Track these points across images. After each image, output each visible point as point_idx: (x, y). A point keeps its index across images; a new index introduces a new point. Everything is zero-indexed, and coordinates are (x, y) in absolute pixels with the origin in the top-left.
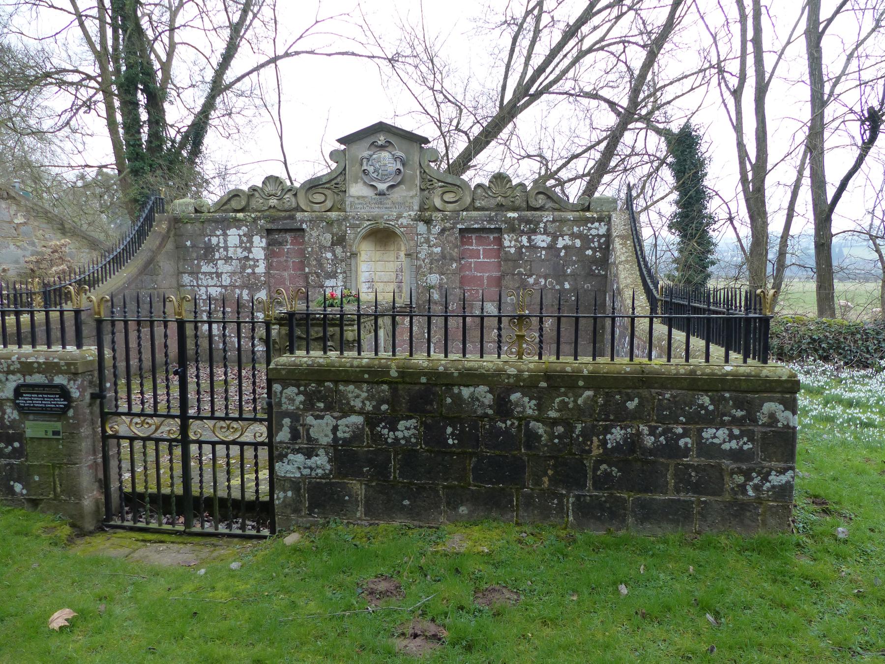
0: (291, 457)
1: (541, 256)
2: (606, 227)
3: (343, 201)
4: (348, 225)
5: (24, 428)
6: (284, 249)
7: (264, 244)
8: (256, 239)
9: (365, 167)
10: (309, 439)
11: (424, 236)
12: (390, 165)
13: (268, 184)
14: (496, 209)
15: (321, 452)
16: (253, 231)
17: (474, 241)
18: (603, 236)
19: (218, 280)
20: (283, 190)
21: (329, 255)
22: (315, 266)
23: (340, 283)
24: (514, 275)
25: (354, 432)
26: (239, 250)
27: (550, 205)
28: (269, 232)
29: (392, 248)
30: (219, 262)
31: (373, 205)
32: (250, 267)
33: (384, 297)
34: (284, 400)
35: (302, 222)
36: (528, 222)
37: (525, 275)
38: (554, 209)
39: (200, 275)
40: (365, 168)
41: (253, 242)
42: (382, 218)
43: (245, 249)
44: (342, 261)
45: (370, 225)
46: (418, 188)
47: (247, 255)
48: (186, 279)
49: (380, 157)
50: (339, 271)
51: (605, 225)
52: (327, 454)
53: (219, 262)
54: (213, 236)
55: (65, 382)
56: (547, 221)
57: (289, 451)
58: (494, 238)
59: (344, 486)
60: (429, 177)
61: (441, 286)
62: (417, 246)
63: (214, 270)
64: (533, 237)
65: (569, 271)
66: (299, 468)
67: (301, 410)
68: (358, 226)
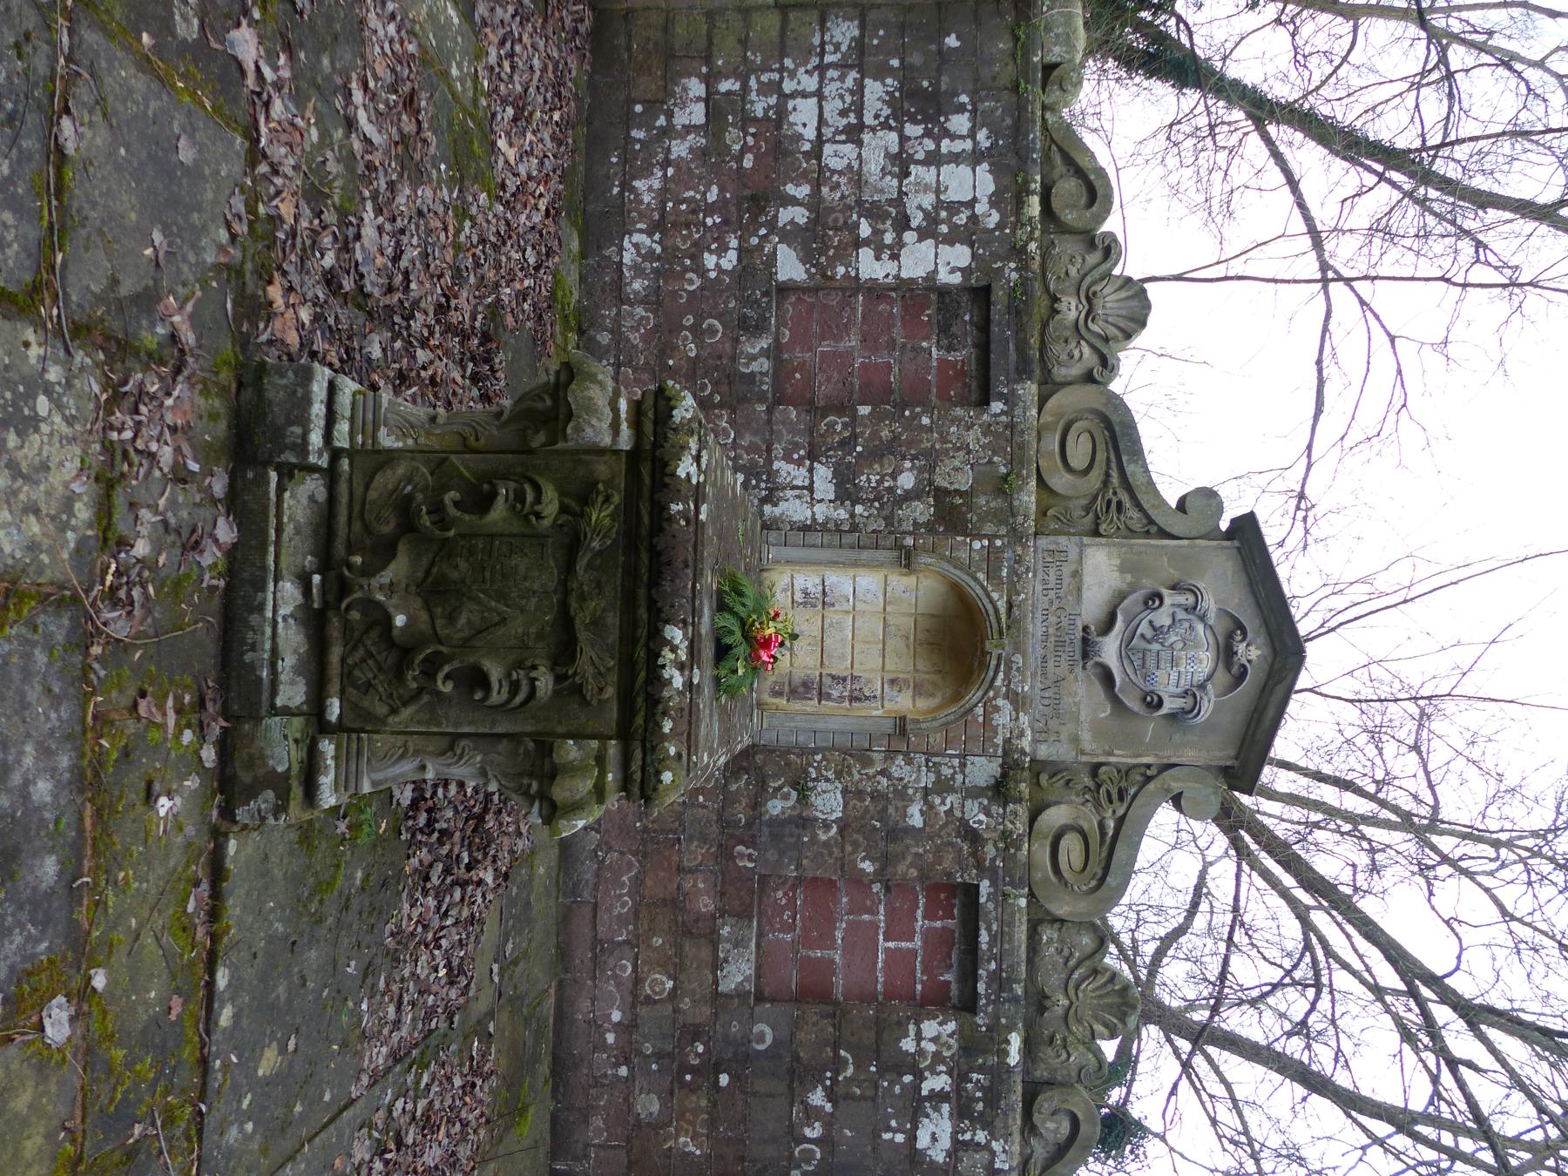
6: (927, 338)
7: (945, 277)
8: (961, 255)
11: (959, 777)
12: (1174, 676)
16: (984, 245)
21: (907, 481)
23: (821, 511)
26: (928, 200)
28: (981, 295)
32: (878, 233)
35: (1011, 400)
36: (993, 1096)
43: (932, 219)
44: (889, 520)
45: (996, 611)
47: (914, 224)
50: (859, 509)
54: (973, 119)
60: (1132, 791)
63: (868, 119)
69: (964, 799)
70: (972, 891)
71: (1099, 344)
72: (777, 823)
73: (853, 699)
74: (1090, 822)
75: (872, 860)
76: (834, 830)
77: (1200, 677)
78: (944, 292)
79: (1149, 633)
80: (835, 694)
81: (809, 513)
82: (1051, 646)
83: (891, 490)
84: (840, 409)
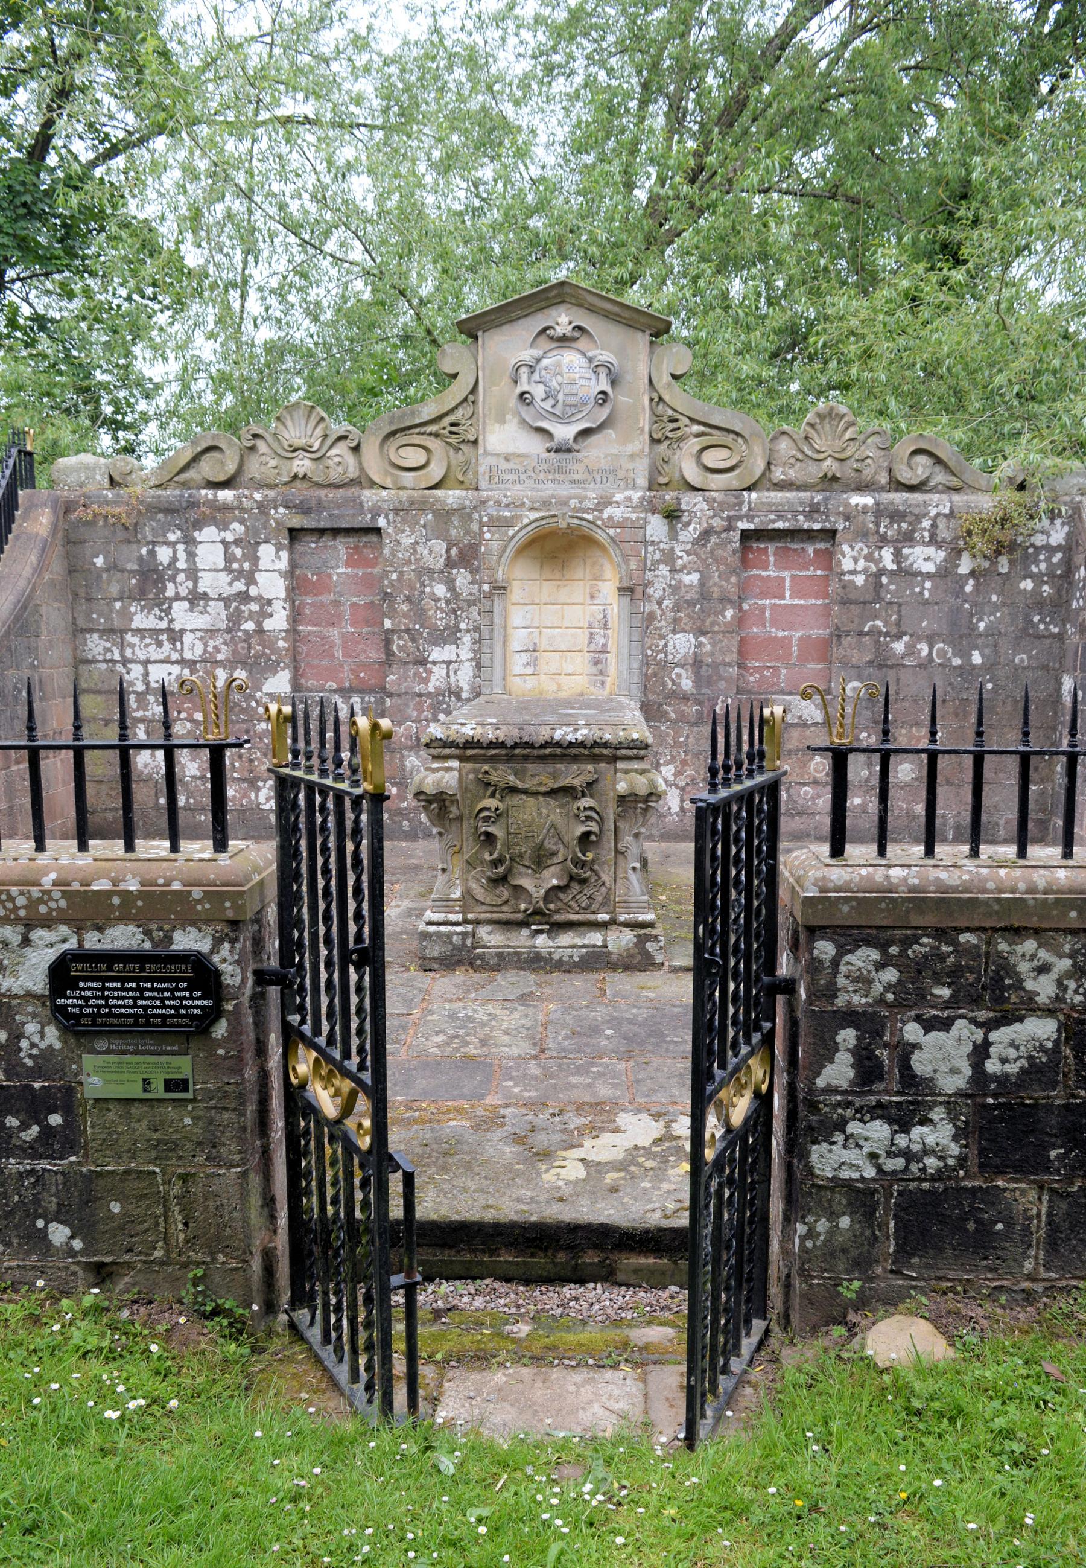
0: (854, 1128)
1: (921, 593)
2: (1066, 528)
3: (466, 466)
4: (485, 519)
5: (80, 1072)
6: (330, 576)
7: (283, 564)
8: (266, 552)
9: (523, 386)
10: (909, 1079)
11: (662, 546)
12: (582, 382)
13: (289, 423)
14: (819, 487)
15: (938, 1114)
16: (257, 533)
17: (772, 559)
18: (1058, 548)
19: (174, 649)
20: (326, 436)
21: (440, 590)
22: (405, 615)
23: (465, 653)
24: (861, 634)
25: (1030, 1058)
26: (224, 578)
27: (940, 477)
28: (294, 534)
29: (579, 574)
30: (176, 605)
31: (542, 476)
33: (559, 685)
34: (841, 981)
36: (896, 516)
37: (887, 634)
38: (950, 489)
39: (129, 637)
40: (526, 388)
41: (257, 559)
42: (566, 504)
43: (239, 574)
44: (471, 603)
45: (537, 520)
46: (647, 436)
47: (244, 588)
48: (95, 645)
49: (558, 365)
50: (463, 626)
51: (1063, 524)
52: (953, 1119)
53: (176, 605)
55: (205, 946)
56: (938, 515)
57: (849, 1113)
58: (816, 551)
59: (992, 1196)
60: (670, 412)
61: (696, 663)
62: (644, 569)
63: (163, 625)
64: (905, 551)
65: (982, 626)
66: (873, 1156)
67: (888, 1006)
68: (508, 523)
69: (677, 541)
70: (746, 535)
71: (329, 442)
72: (698, 681)
73: (605, 627)
74: (694, 444)
75: (724, 609)
76: (702, 639)
77: (583, 362)
78: (293, 565)
79: (551, 402)
80: (602, 641)
81: (467, 664)
82: (562, 477)
83: (448, 602)
84: (388, 642)
